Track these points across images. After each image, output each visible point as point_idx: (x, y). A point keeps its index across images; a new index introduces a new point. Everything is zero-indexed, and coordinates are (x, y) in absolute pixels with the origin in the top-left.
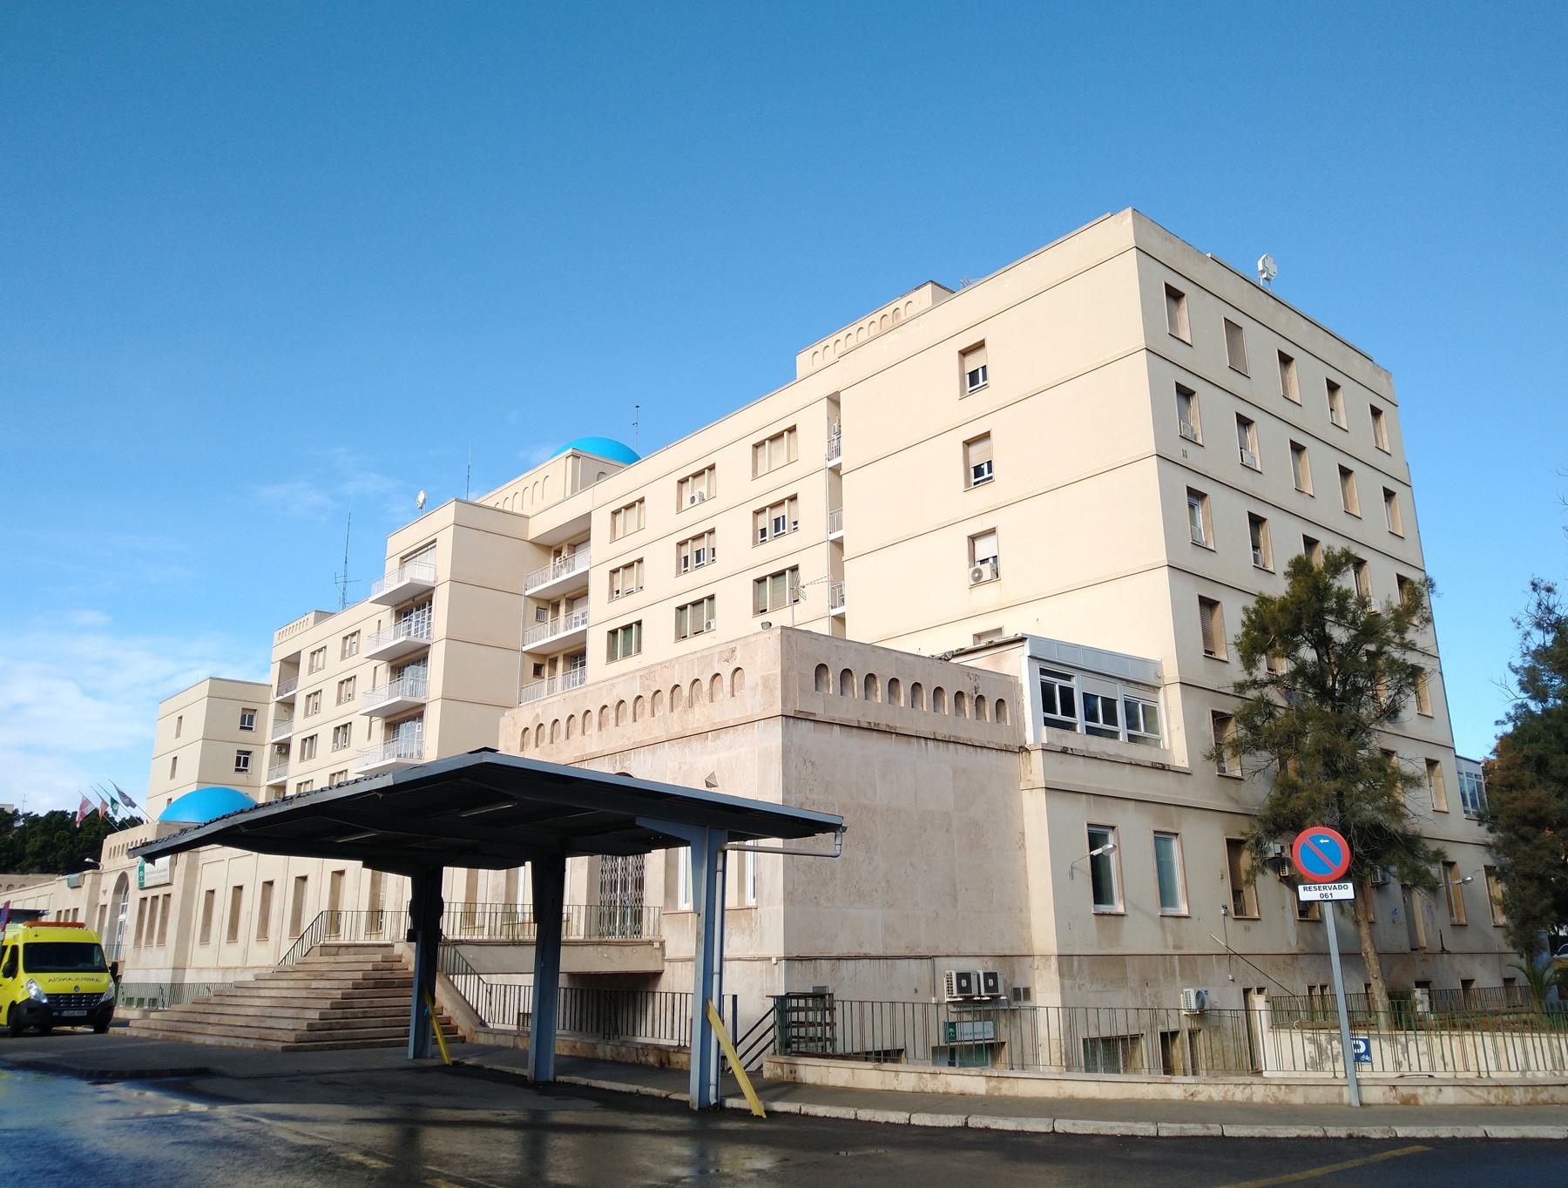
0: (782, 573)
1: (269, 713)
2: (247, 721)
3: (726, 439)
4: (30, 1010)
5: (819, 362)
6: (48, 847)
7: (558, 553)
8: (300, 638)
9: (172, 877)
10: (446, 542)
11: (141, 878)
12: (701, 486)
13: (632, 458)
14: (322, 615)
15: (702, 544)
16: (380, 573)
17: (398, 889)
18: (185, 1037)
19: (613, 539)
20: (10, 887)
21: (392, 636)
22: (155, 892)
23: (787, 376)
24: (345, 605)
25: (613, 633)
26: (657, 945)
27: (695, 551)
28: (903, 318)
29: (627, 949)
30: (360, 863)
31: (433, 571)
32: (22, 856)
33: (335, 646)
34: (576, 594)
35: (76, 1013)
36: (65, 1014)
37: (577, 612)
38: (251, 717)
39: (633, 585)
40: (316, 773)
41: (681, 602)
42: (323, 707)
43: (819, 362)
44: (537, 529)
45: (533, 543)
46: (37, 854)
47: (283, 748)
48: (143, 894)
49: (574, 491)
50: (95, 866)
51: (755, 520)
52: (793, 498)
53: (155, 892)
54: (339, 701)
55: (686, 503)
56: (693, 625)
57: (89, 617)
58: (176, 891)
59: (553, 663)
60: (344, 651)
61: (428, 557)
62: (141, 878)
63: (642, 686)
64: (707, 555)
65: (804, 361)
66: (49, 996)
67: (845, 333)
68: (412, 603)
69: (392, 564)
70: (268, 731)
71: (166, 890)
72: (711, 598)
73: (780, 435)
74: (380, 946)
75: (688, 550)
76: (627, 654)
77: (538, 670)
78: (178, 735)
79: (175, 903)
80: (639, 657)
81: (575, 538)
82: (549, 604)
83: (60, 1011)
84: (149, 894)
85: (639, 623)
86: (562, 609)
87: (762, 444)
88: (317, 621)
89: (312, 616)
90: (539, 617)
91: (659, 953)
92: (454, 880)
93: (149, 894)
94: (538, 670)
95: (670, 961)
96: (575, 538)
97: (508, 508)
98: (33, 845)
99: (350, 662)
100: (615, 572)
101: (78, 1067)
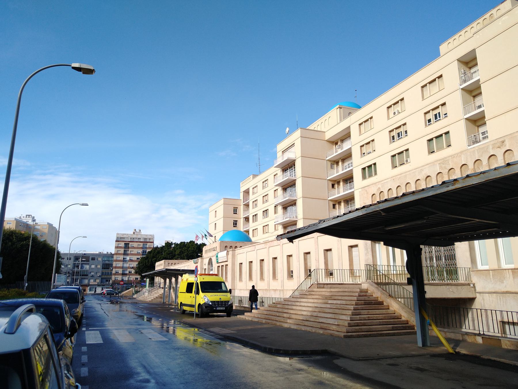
0: (402, 152)
1: (241, 208)
2: (235, 211)
3: (409, 88)
4: (206, 307)
5: (451, 46)
6: (181, 253)
7: (336, 144)
8: (248, 184)
9: (227, 259)
10: (298, 144)
11: (217, 259)
12: (398, 108)
13: (360, 107)
14: (255, 176)
15: (402, 129)
16: (276, 158)
17: (401, 256)
18: (278, 324)
19: (360, 134)
20: (175, 264)
21: (282, 178)
22: (222, 264)
23: (436, 55)
24: (260, 173)
25: (364, 169)
26: (472, 285)
27: (397, 133)
28: (495, 17)
29: (459, 287)
30: (382, 243)
31: (295, 154)
32: (175, 255)
33: (260, 185)
34: (347, 156)
35: (222, 309)
36: (218, 309)
37: (346, 164)
38: (236, 210)
39: (371, 150)
40: (365, 194)
41: (429, 137)
42: (258, 205)
43: (451, 46)
44: (328, 135)
45: (327, 141)
46: (178, 255)
47: (247, 219)
48: (218, 265)
49: (341, 120)
50: (201, 256)
51: (425, 116)
52: (444, 104)
53: (222, 264)
54: (263, 203)
55: (391, 115)
56: (399, 161)
57: (178, 191)
58: (229, 263)
59: (338, 183)
60: (263, 187)
61: (292, 149)
62: (217, 259)
63: (441, 167)
64: (404, 134)
65: (443, 48)
66: (212, 302)
67: (464, 31)
68: (288, 166)
69: (279, 154)
70: (242, 214)
71: (226, 263)
72: (407, 150)
73: (398, 102)
74: (330, 284)
75: (394, 133)
76: (370, 176)
77: (333, 186)
78: (216, 217)
79: (229, 268)
80: (376, 177)
81: (346, 136)
82: (335, 162)
83: (216, 308)
84: (220, 265)
85: (375, 164)
86: (340, 163)
87: (390, 107)
88: (253, 178)
89: (252, 176)
90: (332, 167)
91: (473, 289)
92: (425, 250)
93: (220, 265)
94: (333, 186)
95: (477, 293)
96: (346, 136)
97: (319, 129)
98: (177, 252)
99: (266, 190)
100: (362, 146)
101: (263, 345)
